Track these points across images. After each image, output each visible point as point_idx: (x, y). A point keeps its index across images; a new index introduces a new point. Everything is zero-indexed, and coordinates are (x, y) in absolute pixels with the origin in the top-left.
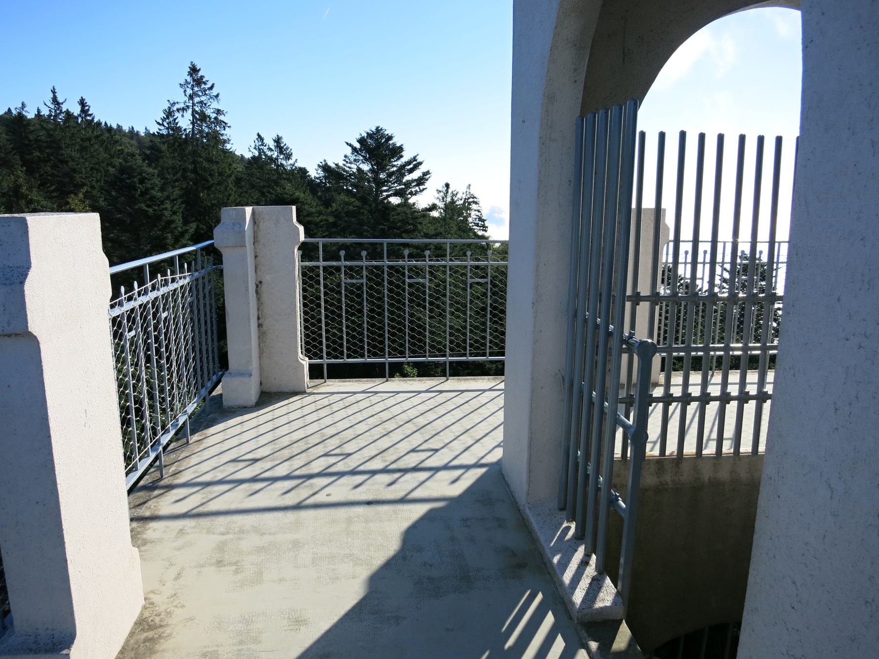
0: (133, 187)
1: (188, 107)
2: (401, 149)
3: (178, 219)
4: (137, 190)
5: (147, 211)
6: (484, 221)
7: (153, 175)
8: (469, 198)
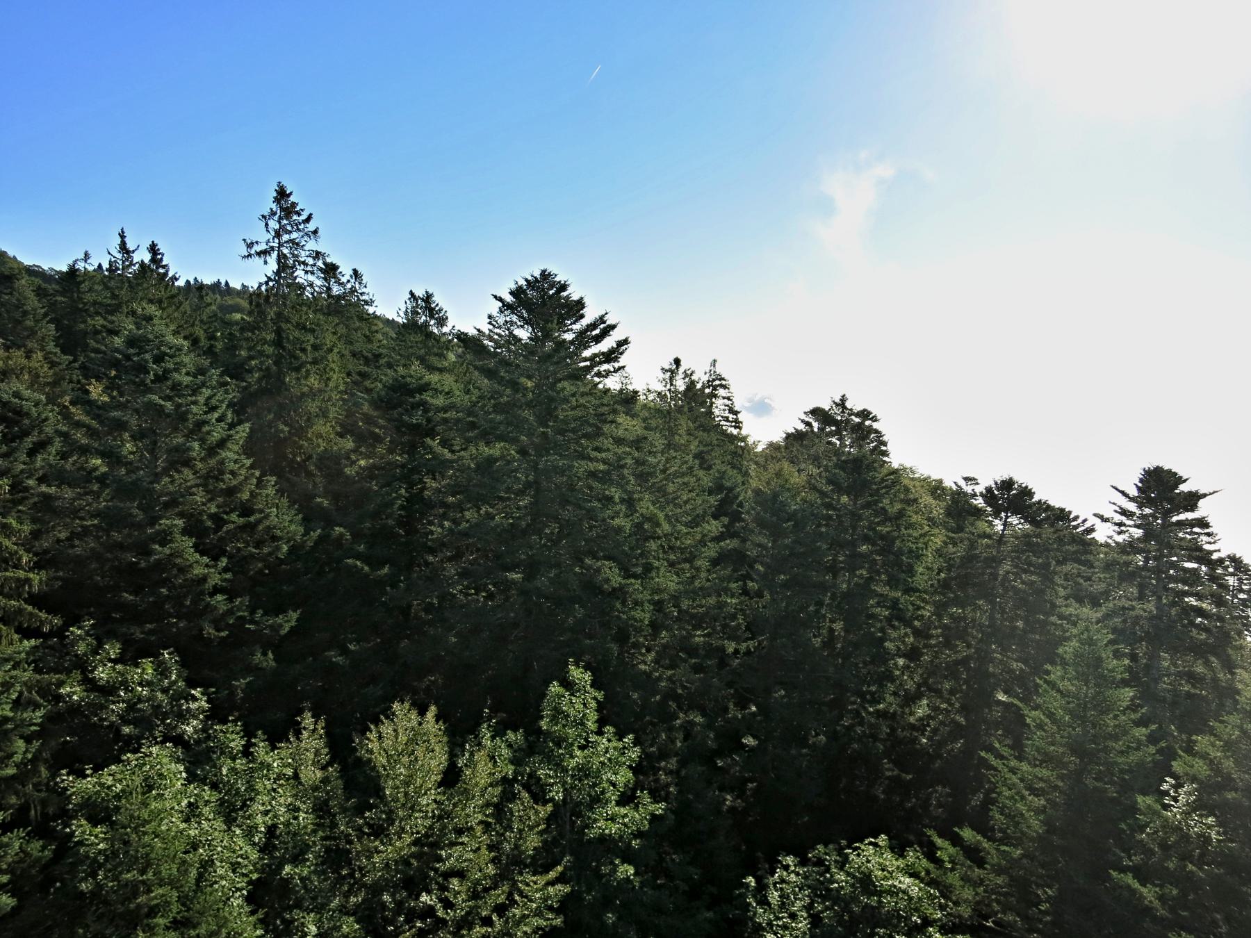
0: (142, 368)
1: (272, 248)
2: (580, 304)
4: (149, 373)
5: (161, 406)
6: (736, 413)
7: (179, 350)
8: (714, 380)
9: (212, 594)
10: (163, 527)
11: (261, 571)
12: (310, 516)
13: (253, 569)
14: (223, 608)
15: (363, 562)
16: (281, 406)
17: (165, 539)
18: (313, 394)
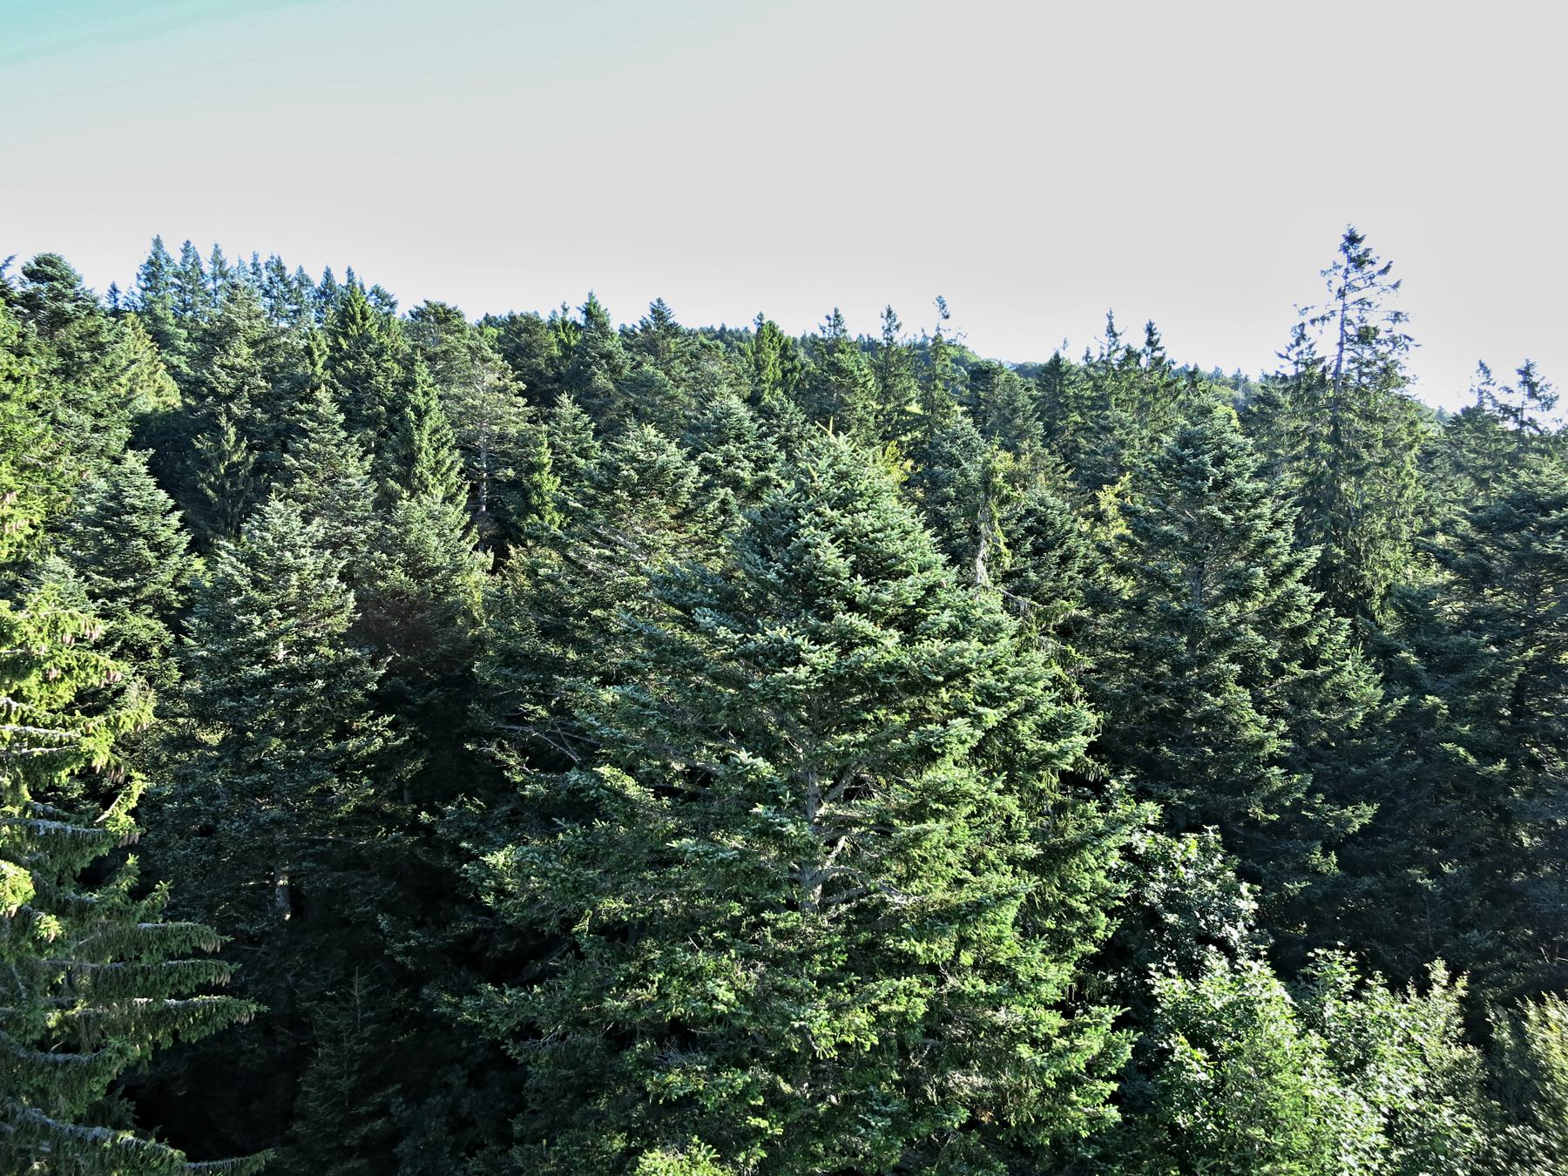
3: (1284, 537)
4: (1207, 479)
9: (1268, 765)
10: (1216, 671)
11: (1324, 745)
12: (1393, 676)
13: (1315, 739)
14: (1278, 784)
15: (1468, 749)
16: (1336, 524)
17: (1218, 686)
18: (1375, 506)
